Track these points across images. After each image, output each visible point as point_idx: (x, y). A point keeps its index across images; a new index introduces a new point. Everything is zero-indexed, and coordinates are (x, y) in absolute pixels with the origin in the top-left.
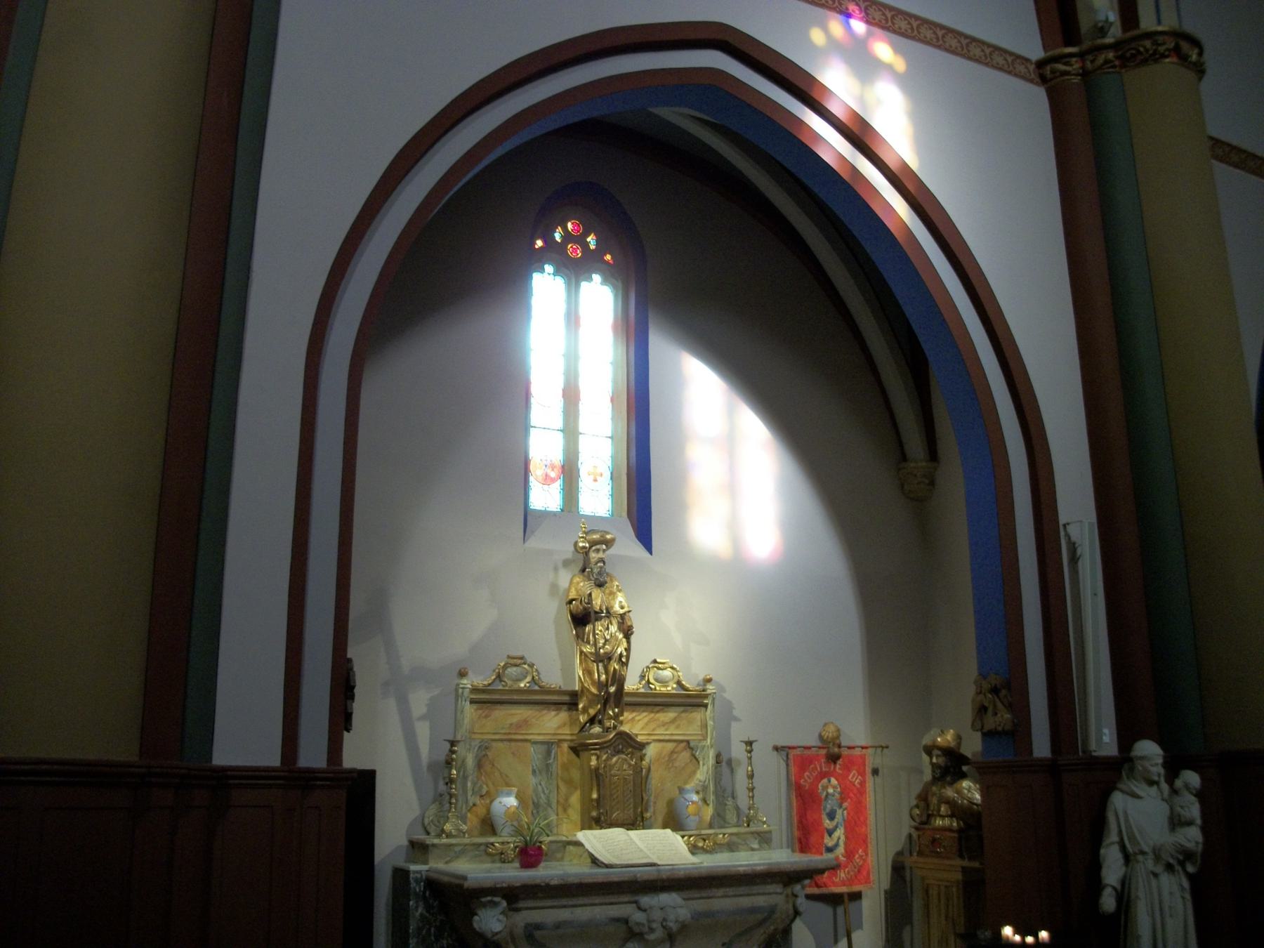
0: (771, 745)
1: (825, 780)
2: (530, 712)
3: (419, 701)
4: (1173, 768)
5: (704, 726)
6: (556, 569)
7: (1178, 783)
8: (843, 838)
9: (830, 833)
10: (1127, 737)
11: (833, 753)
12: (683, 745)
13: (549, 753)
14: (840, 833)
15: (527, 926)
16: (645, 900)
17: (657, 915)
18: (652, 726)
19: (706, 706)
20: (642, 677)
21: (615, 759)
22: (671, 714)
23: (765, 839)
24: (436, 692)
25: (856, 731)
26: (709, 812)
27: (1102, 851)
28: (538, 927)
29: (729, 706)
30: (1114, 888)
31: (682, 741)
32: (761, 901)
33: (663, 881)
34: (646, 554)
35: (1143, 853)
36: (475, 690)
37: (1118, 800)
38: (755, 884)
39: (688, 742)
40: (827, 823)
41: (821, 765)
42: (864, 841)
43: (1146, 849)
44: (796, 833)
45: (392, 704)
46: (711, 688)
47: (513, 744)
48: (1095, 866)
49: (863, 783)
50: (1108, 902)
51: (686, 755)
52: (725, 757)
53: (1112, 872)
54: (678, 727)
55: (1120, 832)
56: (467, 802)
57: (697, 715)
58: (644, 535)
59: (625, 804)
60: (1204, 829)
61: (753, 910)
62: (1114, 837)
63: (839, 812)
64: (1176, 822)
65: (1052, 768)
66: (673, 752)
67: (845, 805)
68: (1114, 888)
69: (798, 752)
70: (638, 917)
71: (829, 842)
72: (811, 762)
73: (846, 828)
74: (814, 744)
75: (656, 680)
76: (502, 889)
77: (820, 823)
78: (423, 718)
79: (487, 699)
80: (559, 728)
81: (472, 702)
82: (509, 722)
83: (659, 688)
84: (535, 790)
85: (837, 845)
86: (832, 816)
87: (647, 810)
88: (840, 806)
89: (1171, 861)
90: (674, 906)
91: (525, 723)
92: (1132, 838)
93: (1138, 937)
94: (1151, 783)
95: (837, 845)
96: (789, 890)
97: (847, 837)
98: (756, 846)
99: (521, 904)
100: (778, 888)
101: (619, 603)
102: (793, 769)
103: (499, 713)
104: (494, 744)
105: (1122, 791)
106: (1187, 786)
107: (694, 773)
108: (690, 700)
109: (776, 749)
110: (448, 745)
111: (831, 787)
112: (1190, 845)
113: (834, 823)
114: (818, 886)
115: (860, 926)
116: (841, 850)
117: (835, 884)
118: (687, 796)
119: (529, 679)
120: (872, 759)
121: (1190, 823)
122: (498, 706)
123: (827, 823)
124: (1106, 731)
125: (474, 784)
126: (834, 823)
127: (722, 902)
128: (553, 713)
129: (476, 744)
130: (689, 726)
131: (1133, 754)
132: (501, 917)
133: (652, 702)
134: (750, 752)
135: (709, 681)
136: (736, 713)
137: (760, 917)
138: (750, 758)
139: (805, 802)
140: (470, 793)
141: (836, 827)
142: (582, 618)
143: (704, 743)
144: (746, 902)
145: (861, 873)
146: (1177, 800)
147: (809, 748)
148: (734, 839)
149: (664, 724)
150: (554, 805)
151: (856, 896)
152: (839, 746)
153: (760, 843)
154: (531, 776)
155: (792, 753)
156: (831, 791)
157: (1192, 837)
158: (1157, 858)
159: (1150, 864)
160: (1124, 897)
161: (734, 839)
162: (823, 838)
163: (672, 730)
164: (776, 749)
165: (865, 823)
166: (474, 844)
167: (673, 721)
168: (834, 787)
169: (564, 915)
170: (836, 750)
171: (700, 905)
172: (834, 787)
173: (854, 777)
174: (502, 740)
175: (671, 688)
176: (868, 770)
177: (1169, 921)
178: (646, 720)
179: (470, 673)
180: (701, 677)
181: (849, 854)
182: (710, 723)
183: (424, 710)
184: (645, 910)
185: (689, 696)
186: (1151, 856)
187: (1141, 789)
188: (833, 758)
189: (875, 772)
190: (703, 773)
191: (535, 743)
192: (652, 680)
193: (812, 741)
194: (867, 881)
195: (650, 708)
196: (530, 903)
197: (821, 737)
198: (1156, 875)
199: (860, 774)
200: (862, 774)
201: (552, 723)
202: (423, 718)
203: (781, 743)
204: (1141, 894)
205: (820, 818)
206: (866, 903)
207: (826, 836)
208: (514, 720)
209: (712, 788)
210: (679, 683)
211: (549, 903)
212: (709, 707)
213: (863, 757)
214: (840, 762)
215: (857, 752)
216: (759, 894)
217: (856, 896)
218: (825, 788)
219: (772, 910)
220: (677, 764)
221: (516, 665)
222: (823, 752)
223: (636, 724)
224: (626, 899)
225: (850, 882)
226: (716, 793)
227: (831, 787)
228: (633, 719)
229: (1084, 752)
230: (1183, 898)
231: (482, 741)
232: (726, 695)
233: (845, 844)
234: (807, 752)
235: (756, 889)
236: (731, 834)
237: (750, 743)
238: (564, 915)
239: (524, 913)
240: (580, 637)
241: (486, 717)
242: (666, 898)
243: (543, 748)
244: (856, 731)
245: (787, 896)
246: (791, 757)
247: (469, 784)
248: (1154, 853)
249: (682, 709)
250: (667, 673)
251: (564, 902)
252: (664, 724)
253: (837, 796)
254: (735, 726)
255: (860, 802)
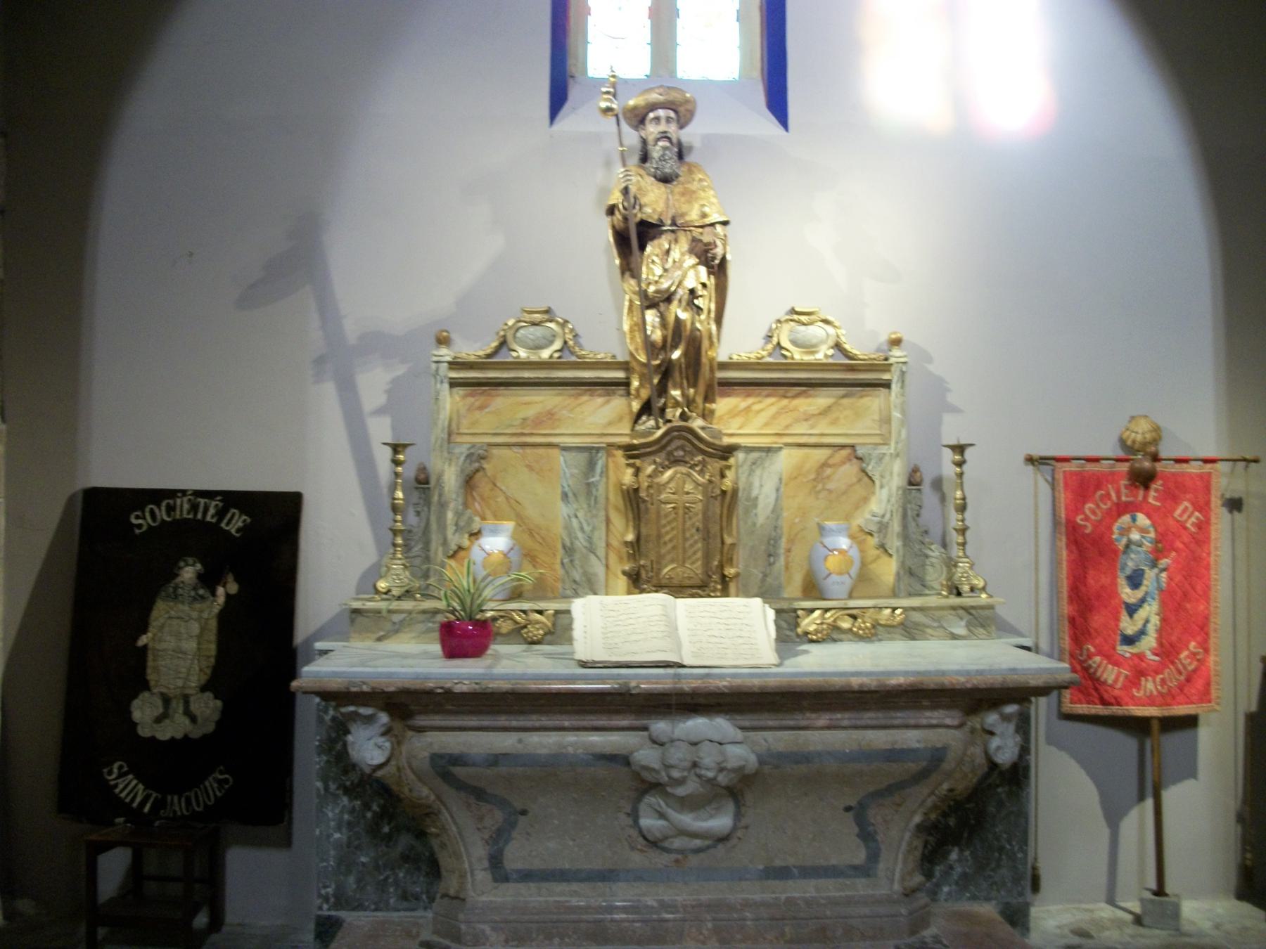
0: (1021, 459)
1: (1126, 519)
2: (560, 398)
3: (374, 384)
5: (886, 420)
6: (608, 164)
8: (1155, 621)
9: (1132, 610)
11: (1143, 471)
12: (845, 452)
13: (591, 465)
14: (1150, 613)
15: (435, 758)
16: (660, 726)
17: (678, 755)
18: (785, 420)
19: (887, 385)
20: (769, 337)
21: (669, 473)
22: (821, 400)
23: (982, 620)
24: (401, 370)
25: (1195, 427)
26: (888, 569)
28: (458, 760)
29: (939, 387)
31: (843, 446)
32: (911, 738)
33: (681, 694)
34: (779, 130)
36: (455, 365)
38: (897, 708)
39: (853, 446)
40: (1127, 594)
41: (1122, 491)
42: (1202, 628)
44: (1066, 609)
45: (329, 390)
46: (897, 354)
47: (529, 451)
49: (1203, 526)
51: (850, 471)
52: (927, 477)
54: (834, 422)
56: (445, 542)
57: (873, 402)
58: (778, 104)
59: (692, 550)
61: (893, 755)
63: (1150, 574)
66: (825, 465)
67: (1164, 562)
69: (1073, 467)
70: (646, 756)
71: (1128, 626)
72: (1098, 486)
73: (1163, 604)
74: (1110, 454)
75: (794, 343)
76: (383, 693)
77: (1114, 593)
78: (380, 411)
79: (485, 378)
80: (610, 424)
81: (454, 384)
82: (521, 415)
83: (798, 355)
84: (568, 528)
85: (1142, 632)
86: (1135, 580)
87: (730, 561)
88: (1154, 565)
90: (724, 742)
91: (550, 416)
95: (1142, 632)
96: (975, 722)
97: (1164, 620)
98: (961, 630)
99: (421, 721)
100: (950, 717)
101: (707, 204)
102: (1062, 497)
103: (504, 401)
104: (495, 451)
107: (865, 500)
108: (856, 377)
109: (1030, 460)
110: (389, 450)
111: (1137, 530)
113: (1139, 594)
114: (1104, 702)
115: (1192, 773)
116: (1148, 643)
117: (1139, 702)
118: (828, 541)
119: (557, 345)
120: (1224, 482)
122: (502, 390)
123: (1127, 594)
125: (458, 515)
126: (1139, 594)
127: (824, 737)
128: (600, 400)
129: (462, 451)
130: (859, 419)
132: (381, 740)
133: (778, 379)
134: (960, 464)
135: (896, 342)
136: (951, 398)
137: (913, 767)
138: (961, 475)
139: (1086, 557)
140: (450, 530)
141: (1143, 601)
142: (633, 237)
143: (884, 449)
144: (879, 739)
145: (1196, 682)
147: (1096, 460)
148: (917, 617)
149: (807, 418)
150: (601, 552)
151: (1190, 722)
152: (1155, 458)
153: (968, 626)
154: (560, 504)
155: (1067, 467)
156: (1135, 536)
157: (182, 564)
161: (917, 617)
162: (1117, 620)
163: (823, 427)
164: (1030, 460)
165: (1206, 595)
166: (424, 612)
167: (825, 412)
168: (1143, 531)
169: (505, 742)
170: (1147, 464)
171: (778, 739)
172: (1143, 531)
173: (1186, 514)
174: (508, 445)
175: (823, 354)
176: (1216, 502)
178: (773, 409)
180: (883, 338)
181: (1167, 651)
182: (896, 414)
183: (381, 400)
184: (662, 744)
185: (851, 369)
188: (1143, 479)
189: (1235, 505)
190: (883, 501)
191: (566, 449)
192: (785, 343)
193: (1107, 448)
194: (1205, 696)
195: (781, 390)
196: (437, 720)
197: (1122, 442)
199: (1198, 508)
200: (1203, 507)
201: (605, 418)
202: (380, 411)
203: (1037, 452)
205: (1114, 584)
206: (1205, 734)
207: (1124, 617)
208: (531, 412)
209: (896, 527)
210: (838, 346)
211: (545, 721)
212: (895, 387)
213: (1206, 480)
214: (1157, 485)
215: (1193, 468)
216: (907, 727)
217: (1190, 722)
218: (1125, 531)
219: (937, 757)
220: (831, 486)
221: (534, 324)
222: (1124, 467)
223: (736, 420)
224: (625, 723)
225: (1167, 698)
226: (905, 537)
227: (1137, 530)
228: (748, 409)
231: (473, 446)
232: (931, 368)
233: (1160, 632)
234: (1091, 467)
235: (900, 717)
236: (905, 609)
237: (960, 449)
238: (505, 742)
239: (431, 737)
240: (629, 267)
241: (481, 408)
242: (697, 725)
243: (583, 457)
244: (1195, 427)
245: (973, 731)
246: (1060, 476)
247: (450, 515)
249: (841, 391)
250: (816, 332)
251: (502, 721)
252: (807, 418)
253: (1147, 544)
254: (948, 420)
255: (1197, 559)
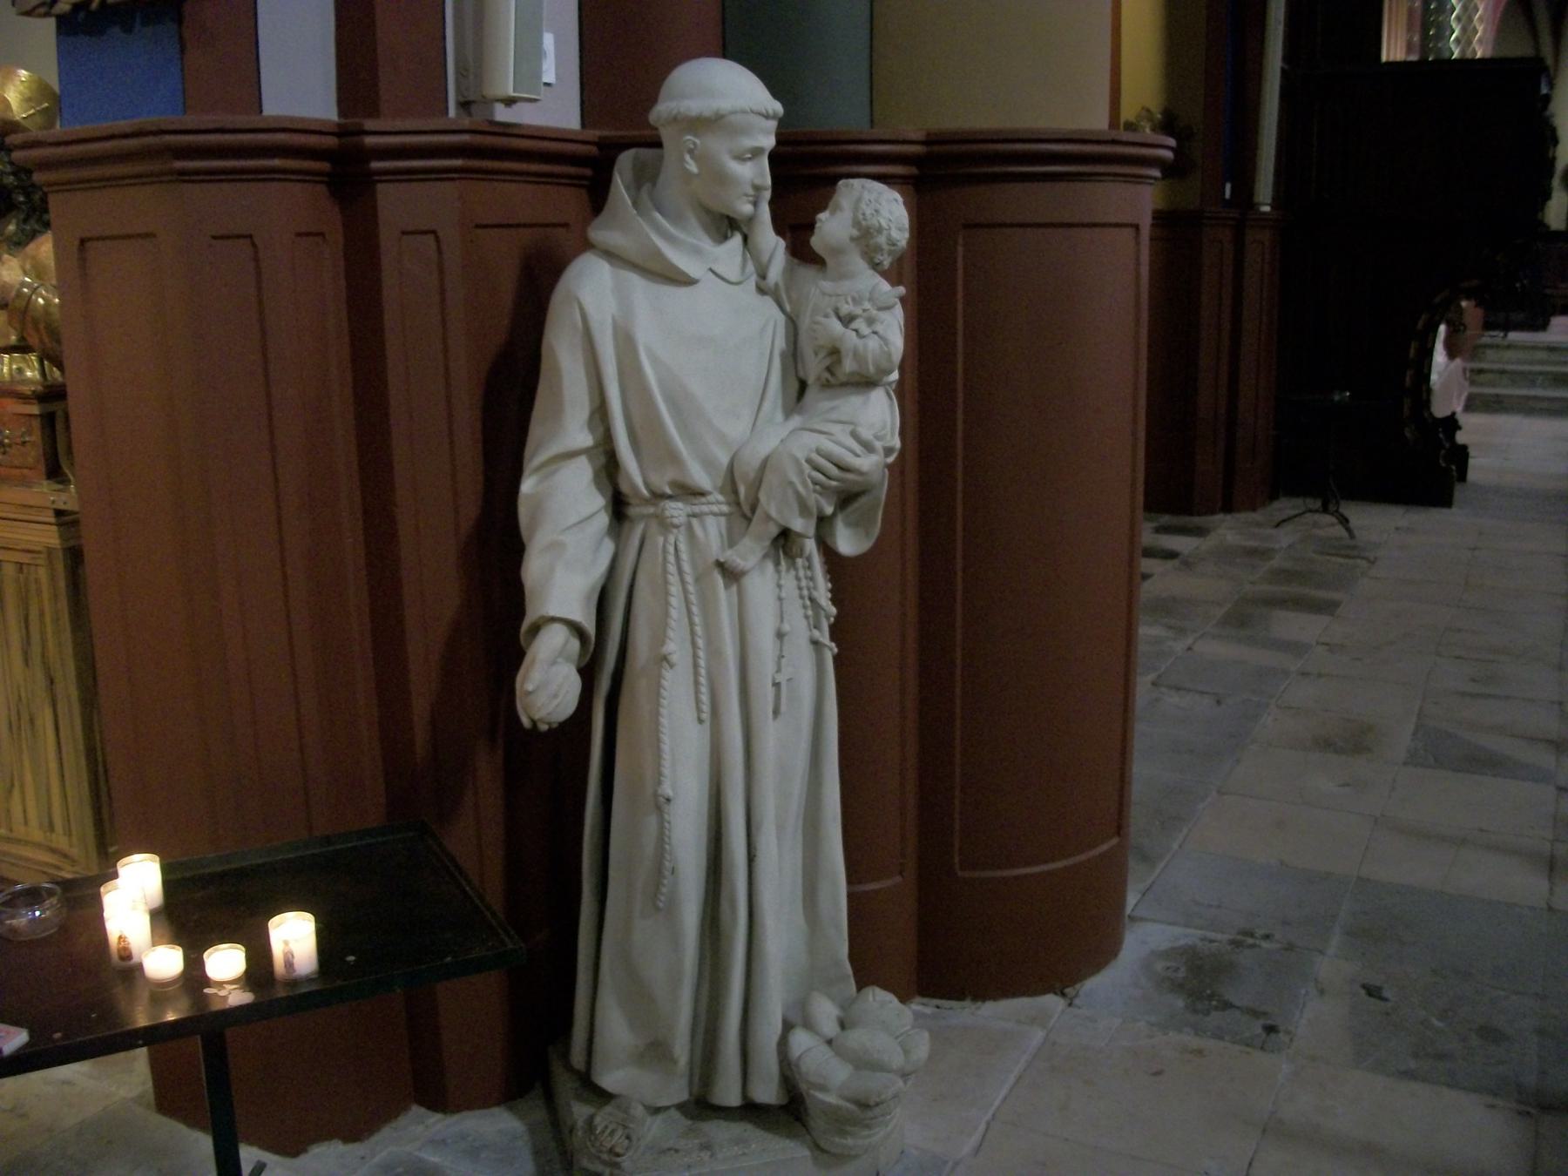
4: (804, 174)
7: (832, 227)
10: (623, 53)
27: (527, 486)
30: (577, 629)
35: (688, 492)
37: (593, 290)
43: (700, 477)
48: (498, 545)
50: (549, 685)
53: (563, 572)
55: (600, 412)
60: (1462, 62)
62: (578, 435)
64: (809, 375)
65: (344, 168)
68: (577, 629)
89: (797, 524)
92: (647, 434)
93: (660, 805)
94: (726, 225)
105: (610, 255)
106: (865, 237)
112: (870, 464)
121: (865, 383)
124: (548, 41)
131: (663, 109)
146: (817, 289)
157: (870, 427)
158: (744, 511)
159: (712, 532)
160: (606, 663)
177: (771, 735)
179: (712, 560)
186: (718, 503)
187: (692, 250)
198: (731, 575)
204: (676, 647)
229: (465, 105)
230: (815, 643)
248: (730, 484)
